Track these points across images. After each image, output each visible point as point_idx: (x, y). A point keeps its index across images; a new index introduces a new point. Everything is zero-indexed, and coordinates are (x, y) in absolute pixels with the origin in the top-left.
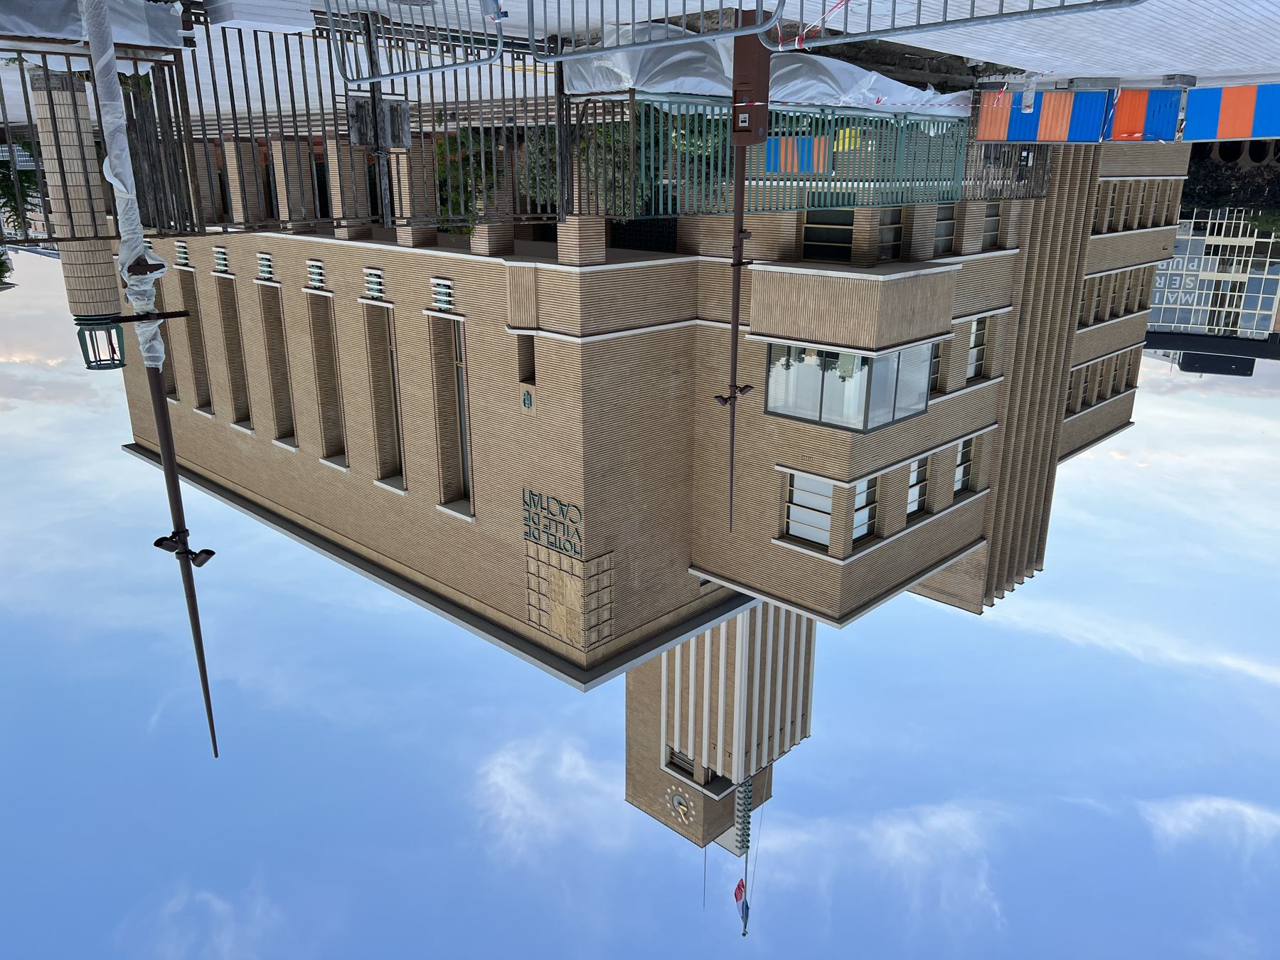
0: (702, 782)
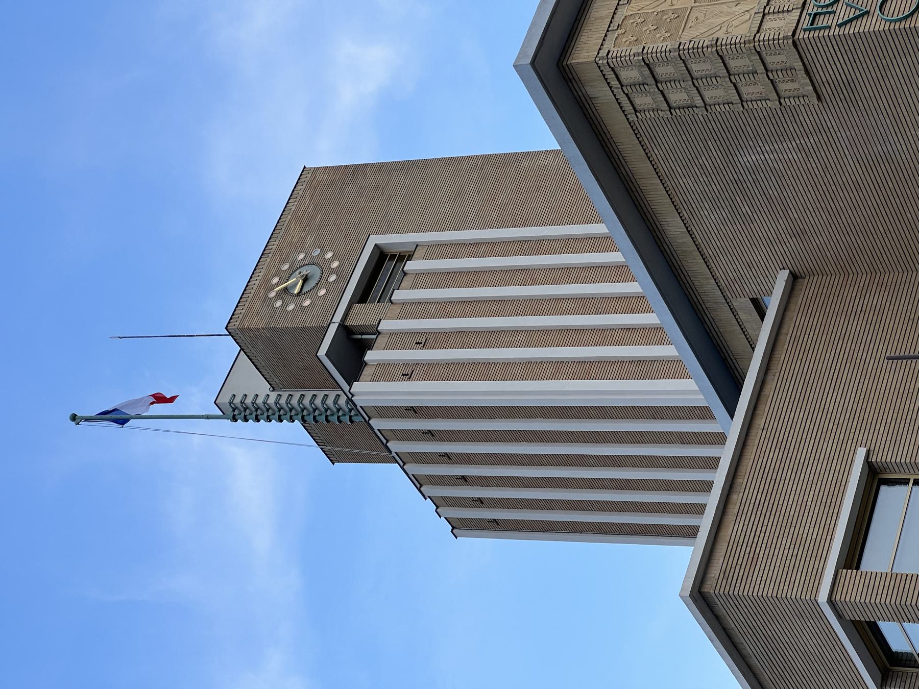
0: (351, 322)
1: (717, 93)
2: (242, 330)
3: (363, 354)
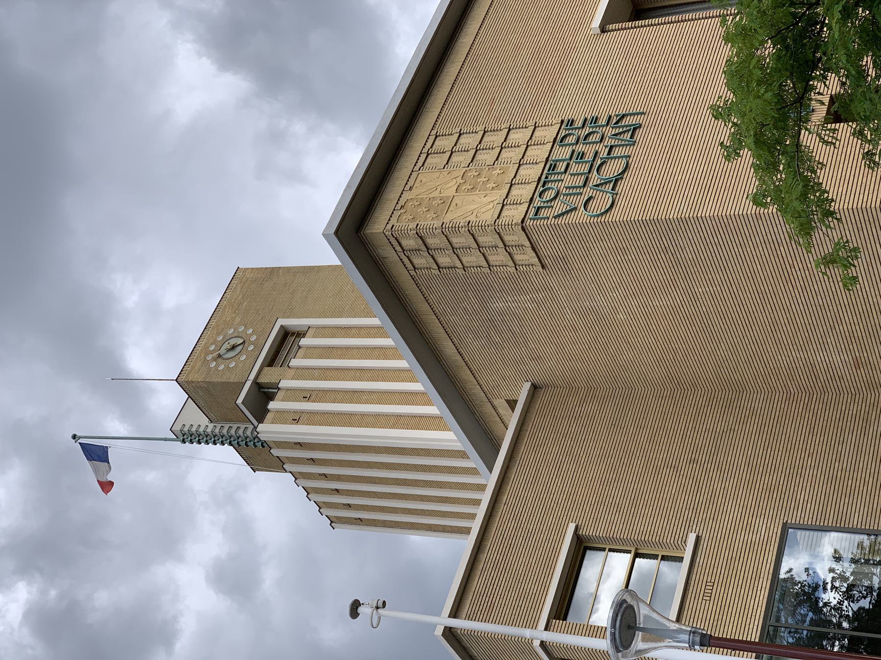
0: (262, 380)
1: (473, 259)
2: (187, 382)
3: (267, 404)
